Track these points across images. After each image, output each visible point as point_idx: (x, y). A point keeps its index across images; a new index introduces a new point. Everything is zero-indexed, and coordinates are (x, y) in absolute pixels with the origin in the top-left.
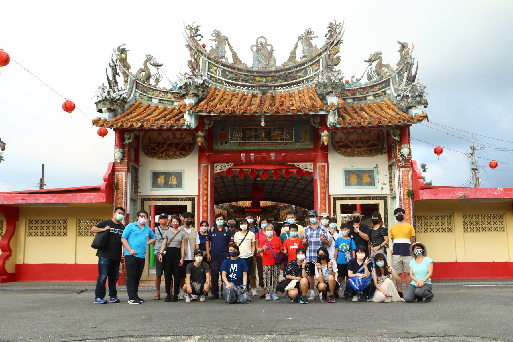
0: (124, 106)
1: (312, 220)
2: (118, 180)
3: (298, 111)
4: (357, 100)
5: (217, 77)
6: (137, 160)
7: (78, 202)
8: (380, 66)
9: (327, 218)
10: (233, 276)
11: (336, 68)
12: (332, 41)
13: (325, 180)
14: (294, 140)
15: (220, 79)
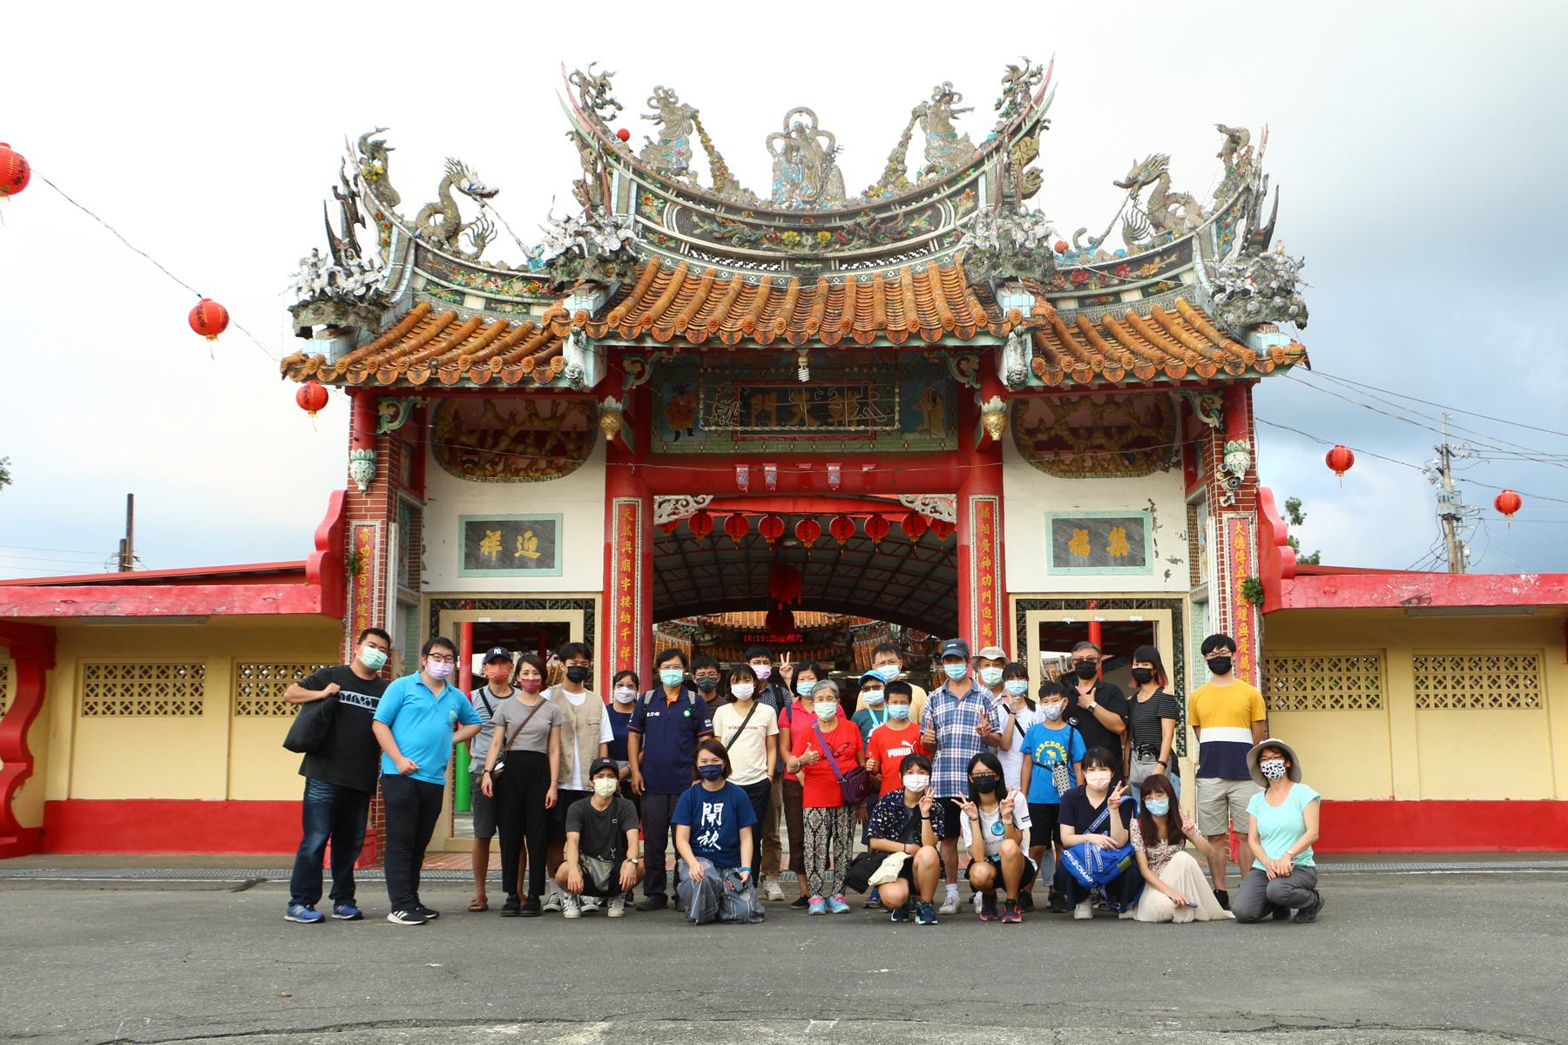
0: (378, 319)
1: (951, 670)
2: (359, 545)
3: (912, 336)
4: (1092, 305)
5: (665, 230)
6: (417, 484)
7: (237, 611)
8: (1164, 199)
9: (1000, 662)
10: (710, 839)
11: (1030, 205)
12: (1017, 122)
13: (992, 548)
14: (897, 426)
15: (671, 238)
